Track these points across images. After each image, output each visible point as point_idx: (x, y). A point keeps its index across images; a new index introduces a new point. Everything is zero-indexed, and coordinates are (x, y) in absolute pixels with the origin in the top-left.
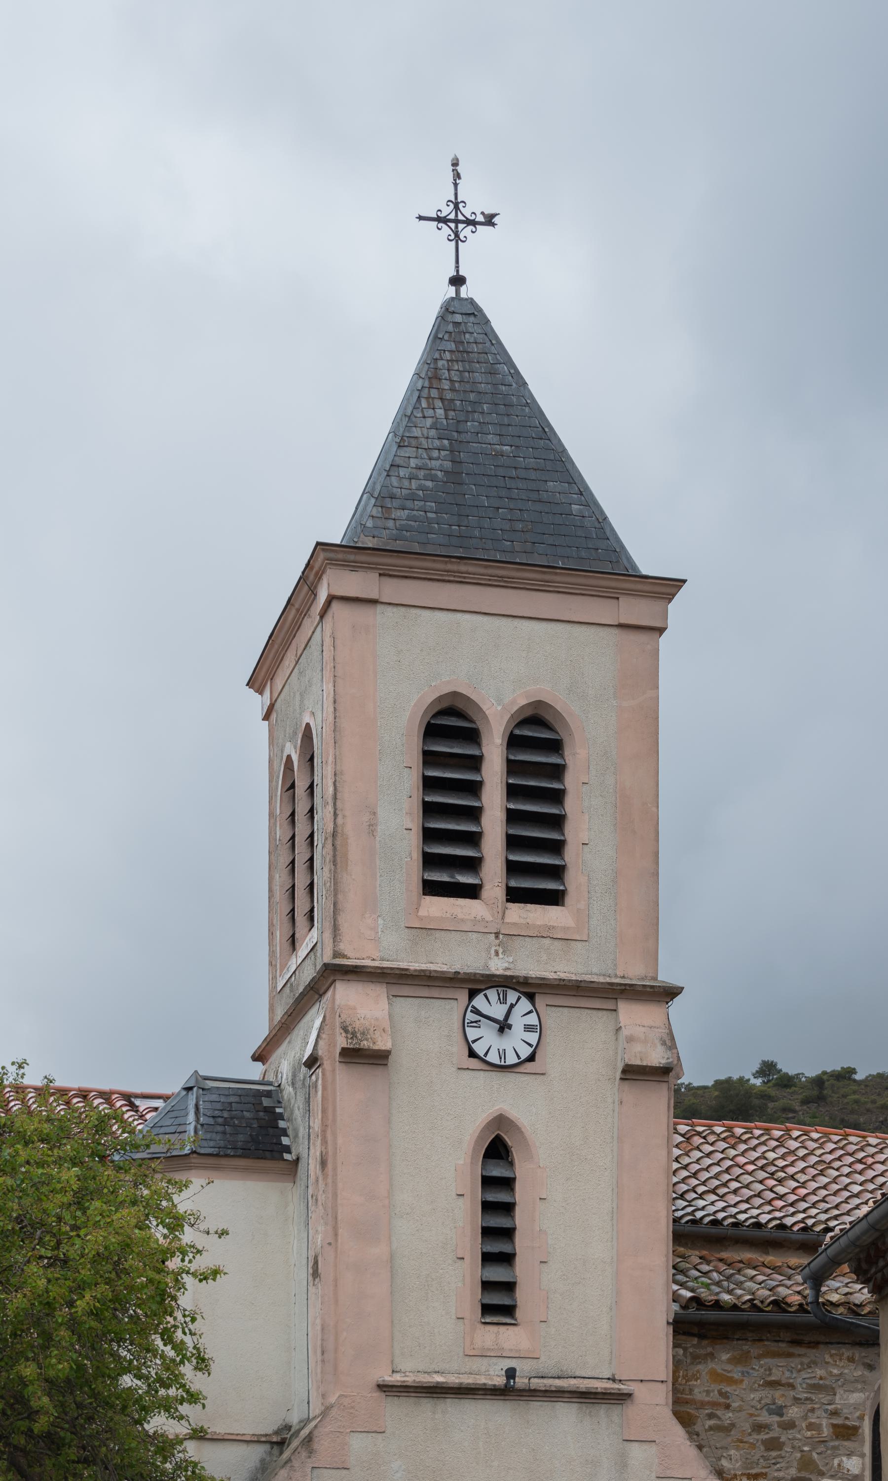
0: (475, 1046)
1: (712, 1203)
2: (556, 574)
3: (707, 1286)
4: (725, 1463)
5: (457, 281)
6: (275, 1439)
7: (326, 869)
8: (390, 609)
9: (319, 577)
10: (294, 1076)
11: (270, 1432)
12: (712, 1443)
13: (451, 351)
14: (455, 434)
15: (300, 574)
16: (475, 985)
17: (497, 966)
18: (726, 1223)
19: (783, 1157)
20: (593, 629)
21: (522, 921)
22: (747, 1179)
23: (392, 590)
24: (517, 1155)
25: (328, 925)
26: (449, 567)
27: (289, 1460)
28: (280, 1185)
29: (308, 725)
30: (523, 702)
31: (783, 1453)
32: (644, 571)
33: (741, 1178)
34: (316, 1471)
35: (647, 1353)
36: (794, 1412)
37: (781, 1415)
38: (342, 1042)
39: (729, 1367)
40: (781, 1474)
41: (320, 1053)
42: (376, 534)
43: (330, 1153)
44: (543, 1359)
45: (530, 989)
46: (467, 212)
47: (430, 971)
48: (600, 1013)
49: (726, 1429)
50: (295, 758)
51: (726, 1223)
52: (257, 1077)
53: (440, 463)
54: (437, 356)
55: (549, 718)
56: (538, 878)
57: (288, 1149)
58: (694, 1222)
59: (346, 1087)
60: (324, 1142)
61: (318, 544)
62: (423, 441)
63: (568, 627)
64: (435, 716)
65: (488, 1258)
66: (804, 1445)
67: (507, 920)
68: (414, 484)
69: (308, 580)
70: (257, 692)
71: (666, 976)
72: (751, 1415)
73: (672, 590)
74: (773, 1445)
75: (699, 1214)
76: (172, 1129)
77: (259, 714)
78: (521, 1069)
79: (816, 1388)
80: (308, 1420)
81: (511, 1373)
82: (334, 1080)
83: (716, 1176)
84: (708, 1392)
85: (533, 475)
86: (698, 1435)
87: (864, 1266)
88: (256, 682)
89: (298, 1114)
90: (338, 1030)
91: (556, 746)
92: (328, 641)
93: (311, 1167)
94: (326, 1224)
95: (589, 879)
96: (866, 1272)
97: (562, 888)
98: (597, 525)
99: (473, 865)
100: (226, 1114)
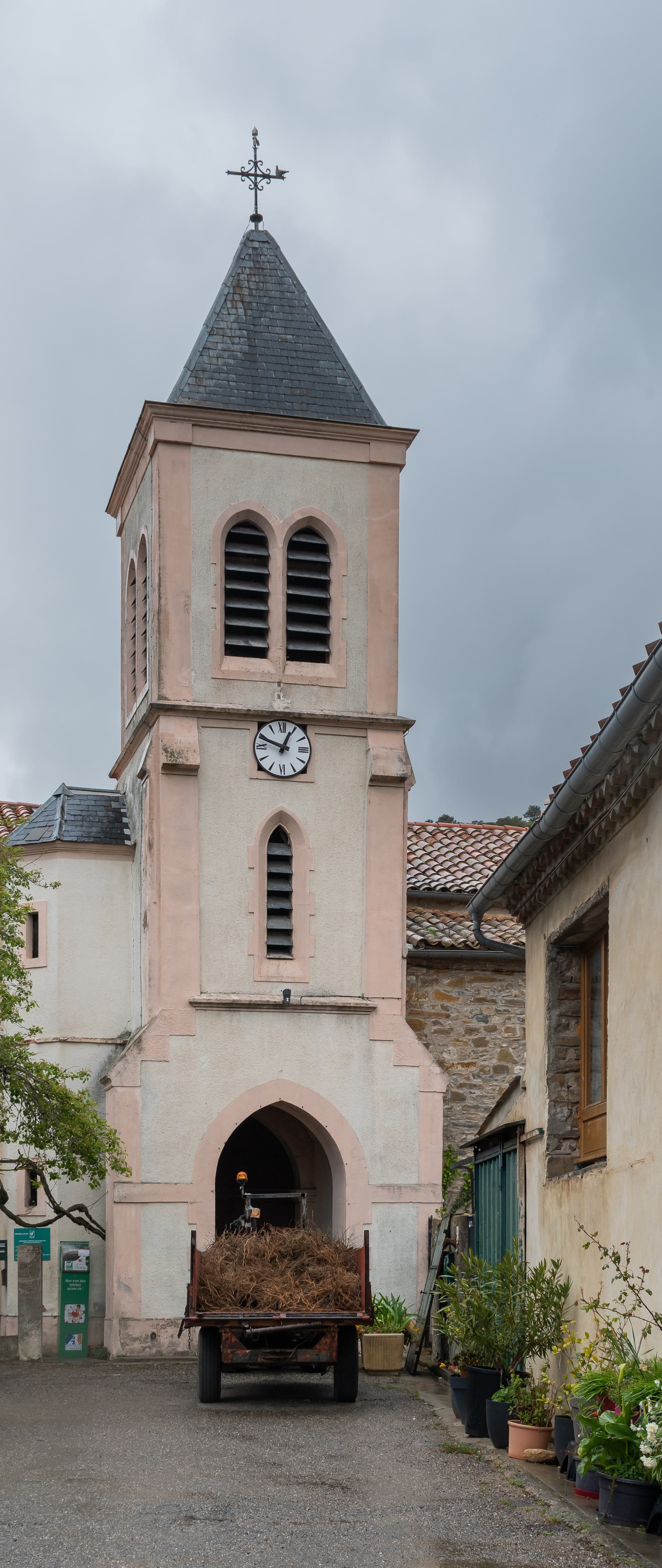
0: (262, 763)
1: (445, 877)
2: (323, 425)
3: (434, 932)
4: (445, 1055)
5: (256, 218)
6: (118, 1042)
7: (154, 637)
8: (200, 450)
9: (148, 427)
10: (134, 785)
11: (115, 1037)
12: (436, 1042)
13: (250, 268)
14: (252, 327)
15: (135, 426)
16: (263, 719)
17: (279, 706)
18: (452, 890)
19: (500, 847)
20: (351, 465)
21: (298, 674)
22: (473, 861)
23: (202, 436)
24: (293, 840)
25: (155, 677)
26: (244, 419)
27: (125, 1055)
28: (122, 863)
29: (143, 535)
30: (299, 517)
31: (487, 1049)
32: (389, 423)
33: (468, 861)
34: (144, 1064)
35: (389, 979)
36: (496, 1020)
37: (487, 1022)
38: (163, 759)
39: (449, 989)
40: (486, 1063)
41: (148, 767)
42: (191, 396)
43: (155, 839)
44: (311, 983)
45: (303, 722)
46: (263, 169)
47: (229, 709)
48: (355, 739)
49: (447, 1032)
50: (136, 561)
51: (452, 890)
52: (113, 788)
53: (240, 347)
54: (240, 271)
55: (318, 528)
56: (310, 642)
57: (128, 838)
58: (429, 889)
59: (168, 791)
60: (151, 830)
61: (146, 402)
62: (228, 331)
63: (332, 464)
64: (234, 527)
65: (272, 913)
66: (504, 1043)
67: (287, 673)
68: (220, 361)
69: (141, 430)
70: (112, 516)
71: (403, 713)
72: (465, 1022)
73: (410, 438)
74: (481, 1043)
75: (433, 884)
76: (44, 824)
77: (115, 531)
78: (296, 779)
79: (512, 1003)
80: (141, 1028)
81: (287, 993)
82: (158, 787)
83: (450, 860)
84: (433, 1006)
85: (309, 356)
86: (426, 1036)
87: (513, 902)
88: (112, 509)
89: (135, 812)
90: (161, 751)
91: (323, 549)
92: (155, 473)
93: (143, 849)
94: (152, 889)
95: (347, 644)
96: (515, 907)
97: (327, 650)
98: (355, 391)
99: (262, 634)
100: (84, 813)
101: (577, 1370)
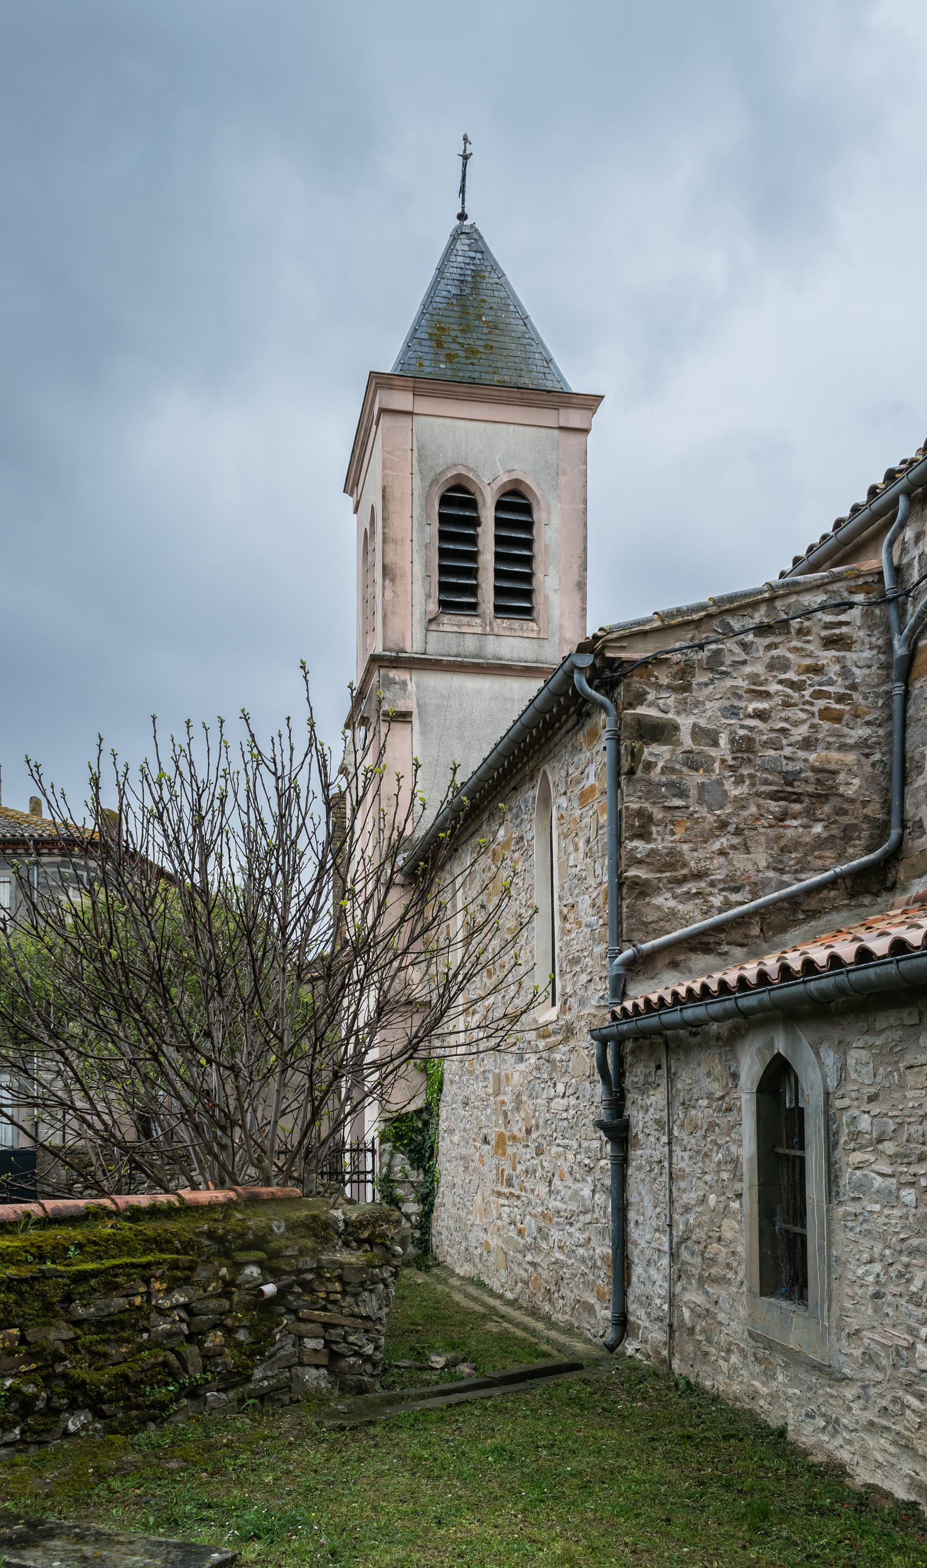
5: (462, 216)
23: (424, 405)
55: (523, 489)
64: (449, 490)
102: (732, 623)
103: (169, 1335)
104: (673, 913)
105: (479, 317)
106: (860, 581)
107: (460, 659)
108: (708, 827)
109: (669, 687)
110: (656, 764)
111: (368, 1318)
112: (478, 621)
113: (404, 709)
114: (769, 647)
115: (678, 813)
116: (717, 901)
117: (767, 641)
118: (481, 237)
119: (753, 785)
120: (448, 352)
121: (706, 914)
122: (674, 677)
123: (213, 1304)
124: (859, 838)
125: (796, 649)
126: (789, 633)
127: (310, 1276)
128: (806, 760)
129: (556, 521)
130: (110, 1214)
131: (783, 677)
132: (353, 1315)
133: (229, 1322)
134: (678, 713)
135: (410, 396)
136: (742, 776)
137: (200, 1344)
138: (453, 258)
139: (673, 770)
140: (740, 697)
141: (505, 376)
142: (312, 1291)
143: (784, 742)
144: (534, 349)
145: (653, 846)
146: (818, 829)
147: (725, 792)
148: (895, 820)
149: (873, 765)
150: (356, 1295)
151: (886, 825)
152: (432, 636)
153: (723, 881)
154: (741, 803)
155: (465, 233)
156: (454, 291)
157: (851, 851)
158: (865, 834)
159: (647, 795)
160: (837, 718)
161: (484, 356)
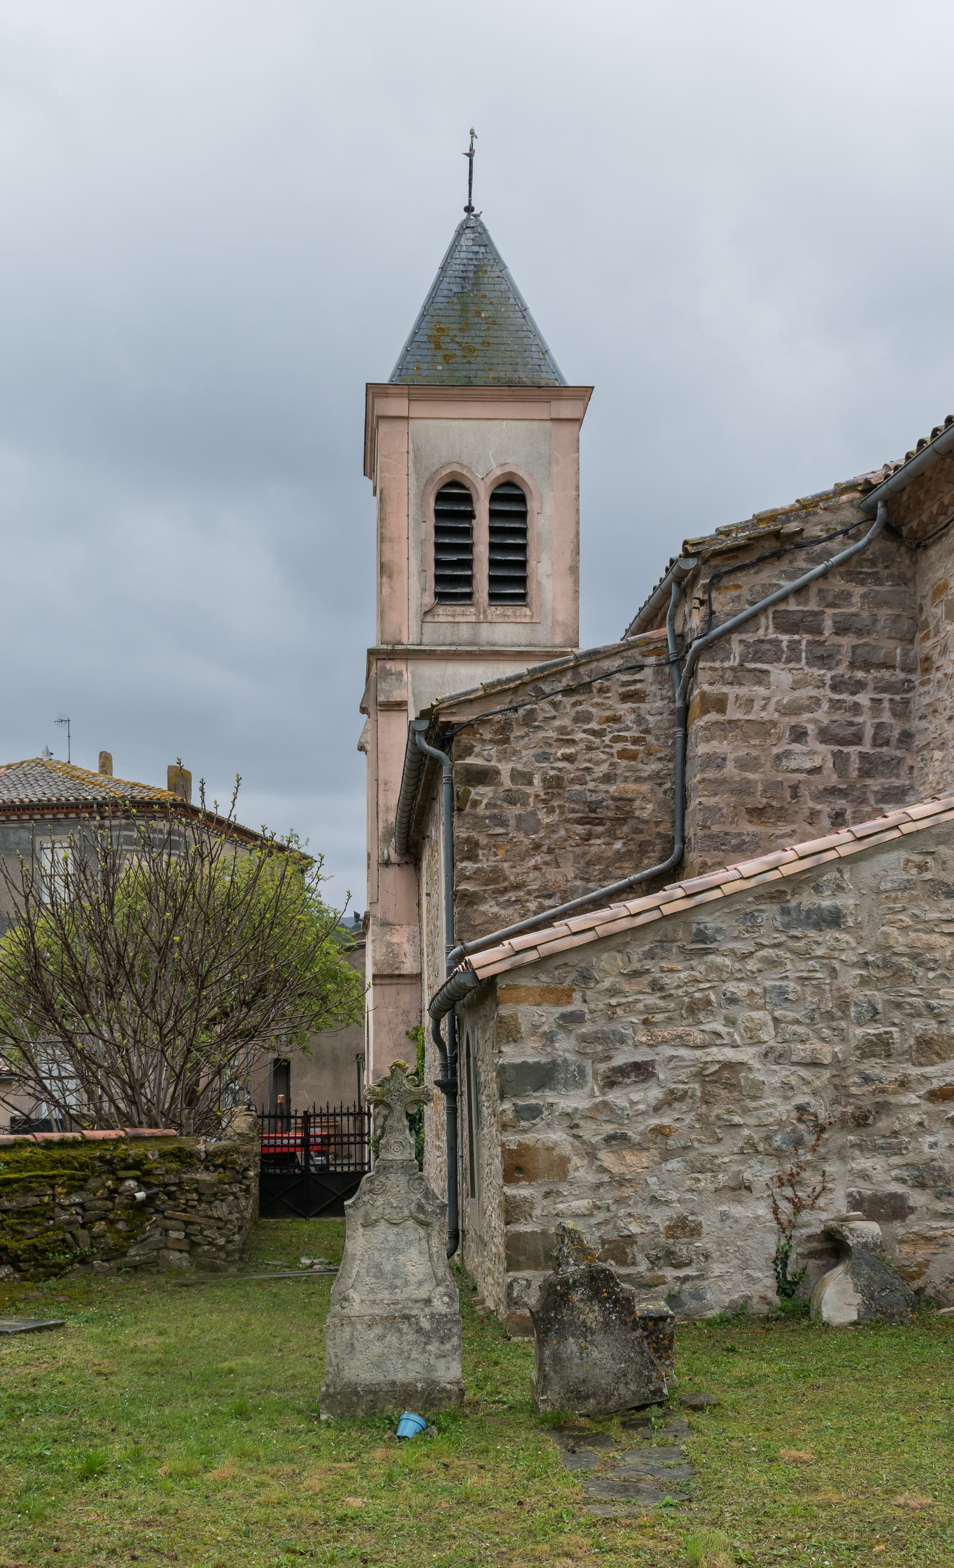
5: (469, 209)
23: (419, 409)
55: (516, 481)
69: (372, 425)
101: (651, 1392)
102: (543, 687)
103: (69, 1223)
104: (496, 917)
105: (478, 313)
106: (652, 647)
107: (453, 648)
108: (524, 849)
109: (491, 741)
110: (481, 802)
111: (219, 1219)
112: (472, 610)
113: (399, 699)
114: (574, 705)
115: (500, 839)
116: (532, 906)
117: (573, 699)
118: (485, 230)
119: (562, 813)
120: (447, 352)
121: (523, 916)
122: (496, 732)
123: (99, 1203)
124: (653, 851)
125: (597, 704)
126: (591, 692)
127: (173, 1188)
128: (607, 792)
129: (548, 509)
130: (31, 1144)
131: (586, 727)
132: (207, 1217)
133: (111, 1216)
134: (499, 761)
135: (405, 402)
136: (553, 807)
137: (90, 1229)
138: (456, 255)
139: (495, 806)
140: (550, 745)
141: (502, 373)
142: (175, 1199)
143: (588, 778)
144: (530, 341)
145: (479, 865)
146: (618, 845)
147: (539, 820)
148: (678, 838)
149: (665, 792)
150: (210, 1203)
151: (672, 841)
152: (428, 628)
153: (538, 890)
154: (552, 829)
155: (472, 226)
156: (455, 289)
157: (646, 861)
158: (658, 848)
159: (474, 826)
160: (633, 757)
161: (481, 354)
